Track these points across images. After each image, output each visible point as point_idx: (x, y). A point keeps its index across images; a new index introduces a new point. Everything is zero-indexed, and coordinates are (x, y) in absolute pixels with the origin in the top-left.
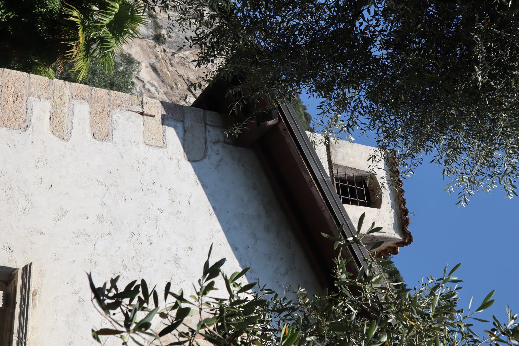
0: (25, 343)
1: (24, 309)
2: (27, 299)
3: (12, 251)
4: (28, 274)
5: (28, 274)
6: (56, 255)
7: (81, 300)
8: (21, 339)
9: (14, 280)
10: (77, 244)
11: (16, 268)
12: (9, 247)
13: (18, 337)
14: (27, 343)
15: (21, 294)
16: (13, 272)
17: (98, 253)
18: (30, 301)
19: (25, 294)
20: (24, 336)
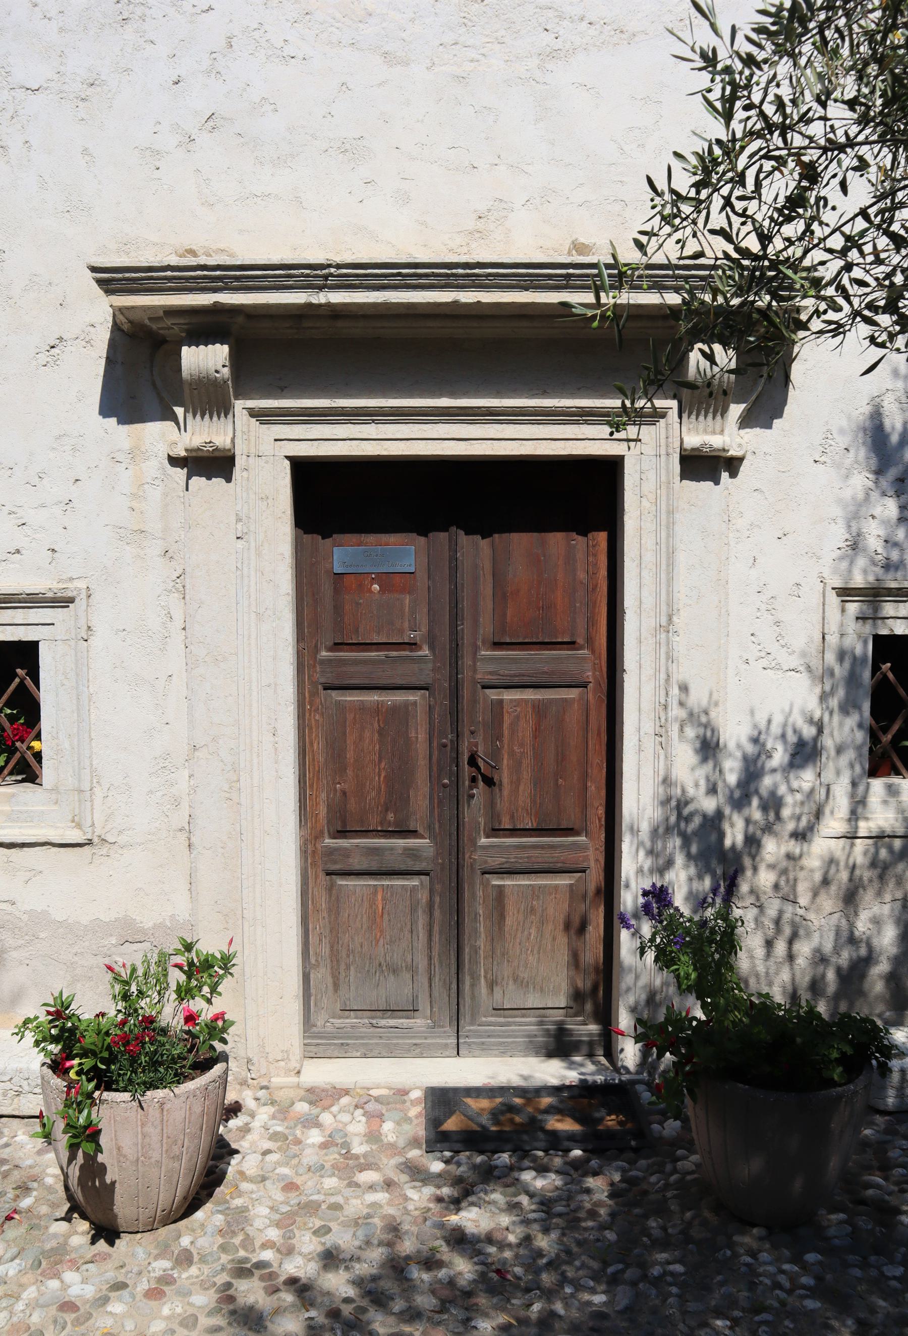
0: (338, 266)
1: (237, 278)
2: (205, 273)
3: (61, 339)
4: (127, 275)
5: (127, 275)
6: (68, 208)
7: (211, 123)
8: (327, 280)
9: (147, 322)
10: (29, 147)
11: (110, 325)
12: (48, 348)
13: (321, 288)
14: (338, 259)
15: (190, 290)
16: (123, 331)
17: (56, 77)
18: (211, 262)
19: (187, 279)
20: (318, 272)
